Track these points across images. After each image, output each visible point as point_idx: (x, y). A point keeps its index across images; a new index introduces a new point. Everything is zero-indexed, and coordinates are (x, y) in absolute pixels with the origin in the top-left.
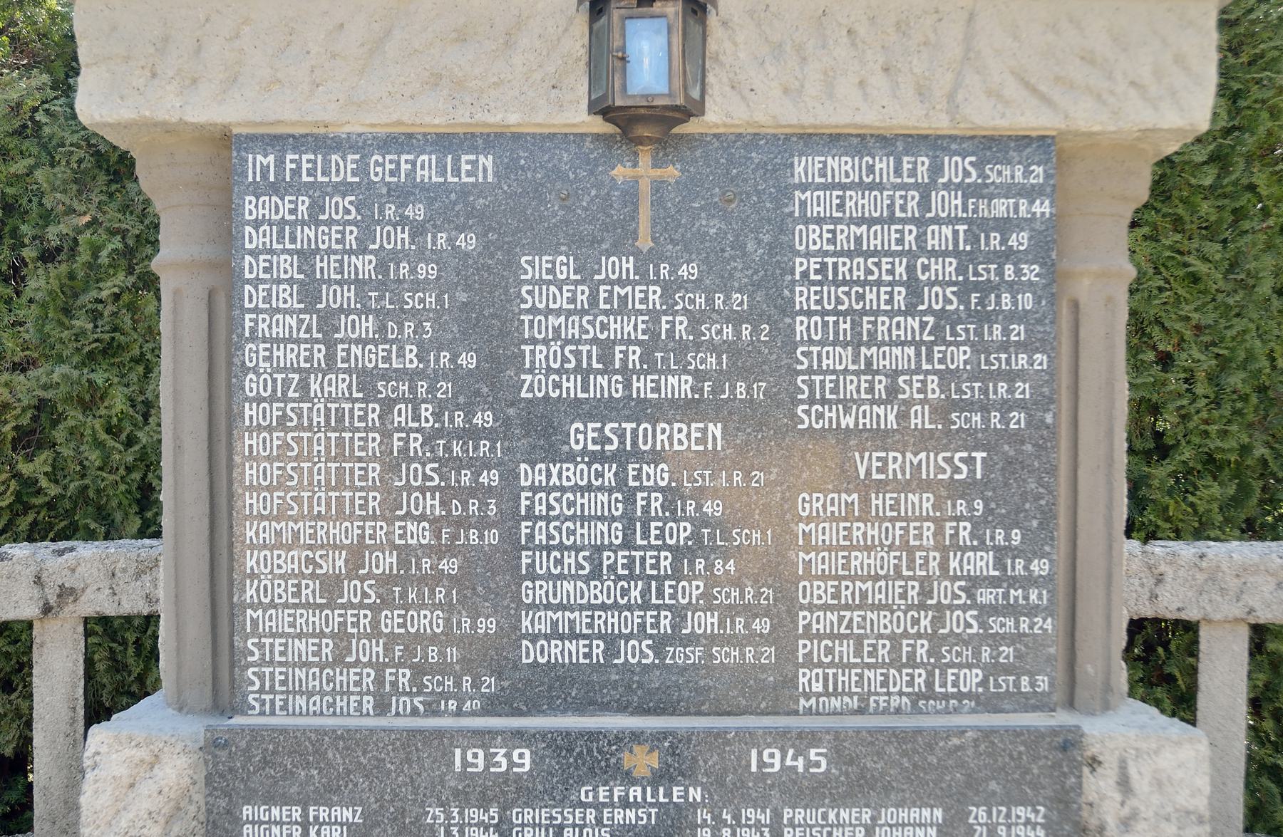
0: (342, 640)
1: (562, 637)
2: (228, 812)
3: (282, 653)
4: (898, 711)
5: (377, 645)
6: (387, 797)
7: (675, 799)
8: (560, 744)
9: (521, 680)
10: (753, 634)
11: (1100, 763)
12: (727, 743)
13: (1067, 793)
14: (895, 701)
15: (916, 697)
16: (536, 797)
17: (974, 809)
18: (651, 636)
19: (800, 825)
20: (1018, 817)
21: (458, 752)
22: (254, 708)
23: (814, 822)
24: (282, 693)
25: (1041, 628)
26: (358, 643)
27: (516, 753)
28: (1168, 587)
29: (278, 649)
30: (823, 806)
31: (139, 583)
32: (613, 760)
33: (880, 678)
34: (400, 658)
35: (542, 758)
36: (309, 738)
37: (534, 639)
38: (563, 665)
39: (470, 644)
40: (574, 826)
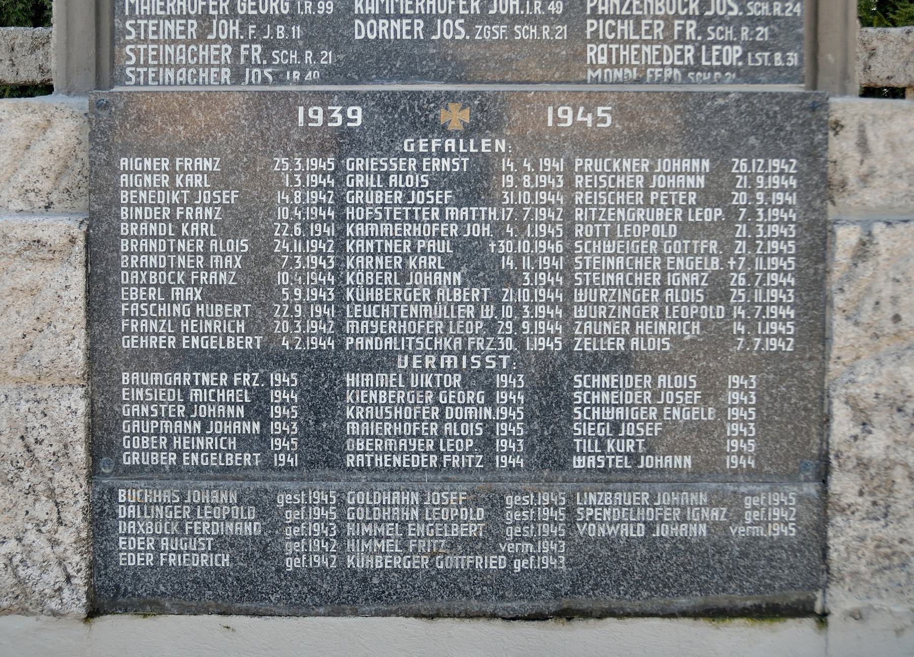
0: (204, 21)
1: (388, 17)
2: (108, 164)
3: (155, 33)
4: (671, 81)
5: (234, 24)
6: (241, 149)
7: (483, 150)
8: (388, 102)
9: (353, 54)
10: (549, 14)
11: (842, 127)
12: (527, 101)
13: (816, 148)
14: (668, 73)
15: (685, 70)
16: (366, 148)
17: (737, 160)
18: (463, 16)
19: (588, 173)
20: (774, 168)
21: (301, 109)
22: (130, 79)
23: (600, 170)
24: (154, 66)
25: (791, 11)
26: (218, 23)
27: (350, 110)
28: (879, 59)
29: (151, 29)
30: (608, 156)
31: (33, 56)
32: (431, 116)
33: (655, 53)
34: (253, 35)
35: (372, 114)
36: (177, 99)
37: (365, 18)
38: (389, 41)
39: (312, 24)
40: (398, 173)
